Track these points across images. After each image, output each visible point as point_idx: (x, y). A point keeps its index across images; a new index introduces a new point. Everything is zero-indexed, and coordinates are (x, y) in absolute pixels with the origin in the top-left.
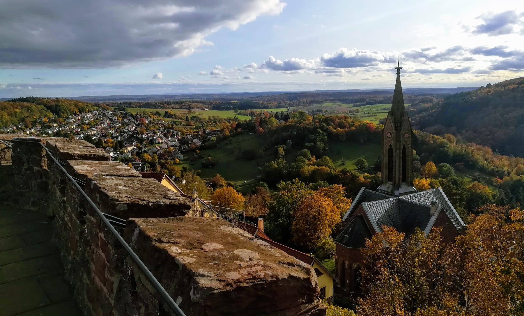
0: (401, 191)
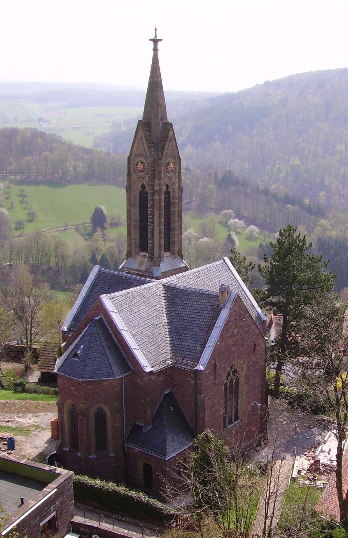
0: (164, 267)
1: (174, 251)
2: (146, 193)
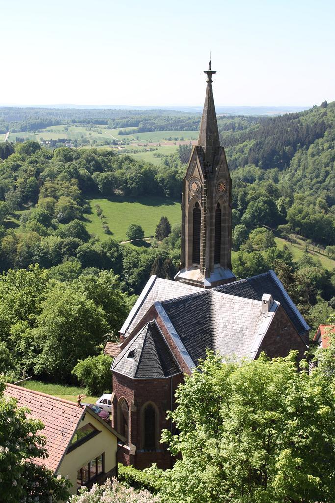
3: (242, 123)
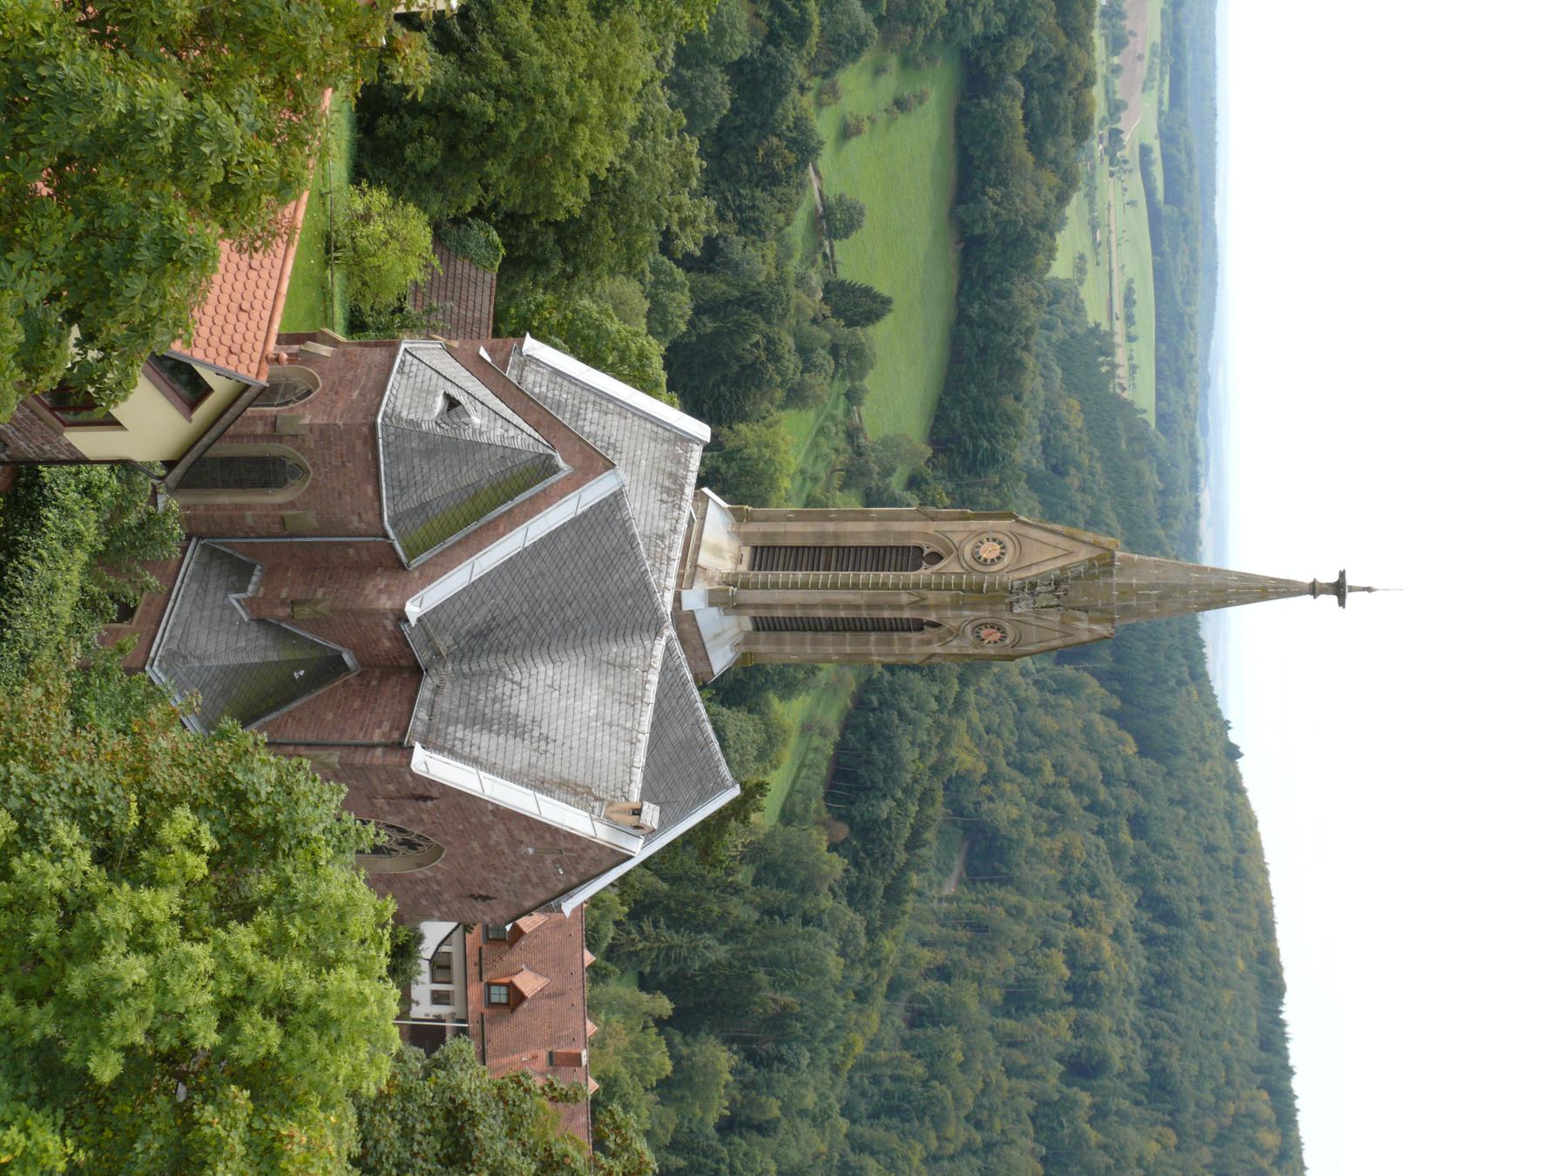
1: (757, 642)
2: (917, 567)
3: (1181, 516)
